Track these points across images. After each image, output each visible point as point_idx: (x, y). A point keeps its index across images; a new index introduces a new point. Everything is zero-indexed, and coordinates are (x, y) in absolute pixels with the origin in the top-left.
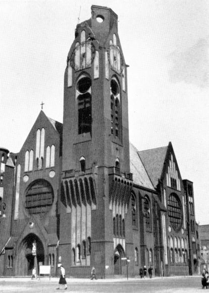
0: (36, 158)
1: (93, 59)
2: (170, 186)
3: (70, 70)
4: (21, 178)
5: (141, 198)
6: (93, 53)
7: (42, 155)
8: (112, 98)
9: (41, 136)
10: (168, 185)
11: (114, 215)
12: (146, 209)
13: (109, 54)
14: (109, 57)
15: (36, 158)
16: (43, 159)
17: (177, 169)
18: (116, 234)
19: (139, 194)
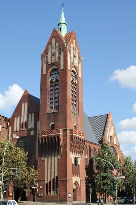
1: (59, 57)
2: (109, 141)
6: (60, 53)
7: (26, 119)
9: (25, 107)
13: (70, 53)
14: (71, 55)
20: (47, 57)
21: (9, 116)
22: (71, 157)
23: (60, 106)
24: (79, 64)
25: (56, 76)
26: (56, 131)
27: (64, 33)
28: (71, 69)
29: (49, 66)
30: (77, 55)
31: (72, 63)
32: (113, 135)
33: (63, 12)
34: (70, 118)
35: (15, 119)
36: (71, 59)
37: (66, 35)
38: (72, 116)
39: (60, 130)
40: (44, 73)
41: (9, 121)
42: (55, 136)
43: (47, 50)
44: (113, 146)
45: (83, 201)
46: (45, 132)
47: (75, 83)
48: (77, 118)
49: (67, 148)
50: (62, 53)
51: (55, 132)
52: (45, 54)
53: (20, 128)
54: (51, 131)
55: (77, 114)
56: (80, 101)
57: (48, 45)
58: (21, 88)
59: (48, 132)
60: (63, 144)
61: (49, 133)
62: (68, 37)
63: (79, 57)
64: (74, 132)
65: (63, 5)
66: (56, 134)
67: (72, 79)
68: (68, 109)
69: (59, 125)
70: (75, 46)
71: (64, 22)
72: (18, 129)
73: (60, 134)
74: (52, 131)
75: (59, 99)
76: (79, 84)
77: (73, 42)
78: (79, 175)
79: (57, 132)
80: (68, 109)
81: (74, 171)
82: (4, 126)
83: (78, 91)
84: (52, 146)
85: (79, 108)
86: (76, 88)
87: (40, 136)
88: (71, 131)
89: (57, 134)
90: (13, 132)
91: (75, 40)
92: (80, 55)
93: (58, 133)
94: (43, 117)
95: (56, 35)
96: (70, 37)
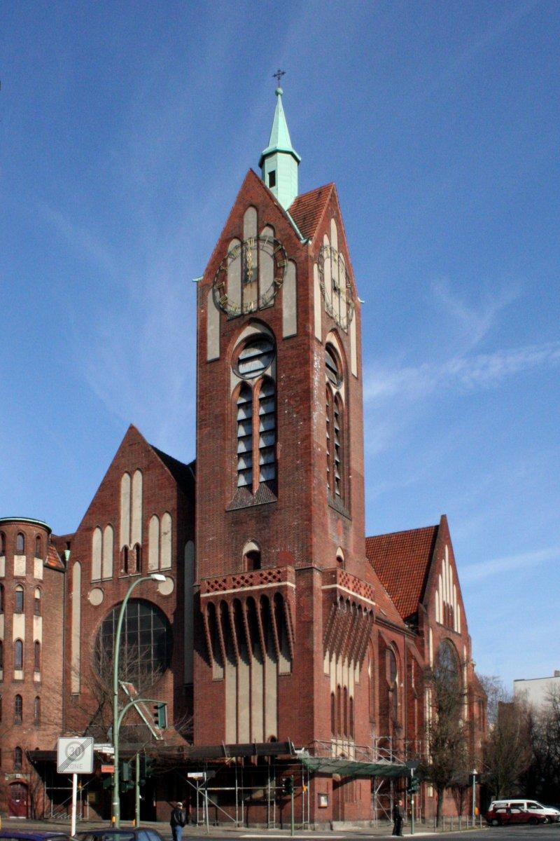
0: (121, 547)
1: (277, 287)
2: (442, 623)
3: (214, 317)
4: (84, 597)
5: (383, 648)
6: (279, 272)
7: (137, 539)
8: (329, 390)
9: (133, 488)
10: (437, 620)
11: (333, 688)
12: (393, 674)
13: (321, 272)
14: (322, 279)
15: (121, 547)
16: (141, 550)
17: (456, 581)
18: (336, 731)
19: (380, 637)
20: (223, 290)
21: (65, 526)
22: (326, 671)
23: (281, 480)
24: (349, 321)
25: (271, 379)
26: (270, 574)
27: (286, 193)
28: (324, 336)
29: (231, 323)
30: (342, 285)
31: (328, 316)
32: (453, 602)
33: (280, 106)
34: (323, 526)
35: (97, 534)
36: (323, 295)
37: (299, 201)
38: (329, 521)
39: (286, 571)
40: (213, 352)
41: (69, 544)
42: (267, 594)
43: (221, 257)
44: (451, 638)
45: (363, 820)
46: (225, 581)
47: (338, 393)
48: (346, 528)
49: (315, 638)
50: (291, 269)
51: (266, 578)
52: (216, 275)
53: (115, 571)
54: (247, 577)
55: (346, 513)
56: (353, 464)
57: (225, 242)
58: (175, 483)
59: (238, 578)
60: (299, 621)
61: (238, 583)
62: (313, 207)
63: (351, 293)
64: (339, 580)
65: (279, 75)
66: (271, 585)
67: (327, 380)
68: (316, 493)
69: (278, 553)
70: (335, 245)
71: (289, 147)
72: (108, 573)
73: (286, 587)
74: (251, 577)
75: (279, 453)
76: (351, 400)
77: (330, 231)
78: (352, 736)
79: (220, 586)
80: (316, 493)
81: (336, 709)
82: (52, 564)
83: (346, 426)
84: (260, 627)
85: (349, 493)
86: (340, 433)
87: (203, 595)
88: (331, 577)
89: (275, 584)
90: (87, 584)
91: (338, 224)
92: (352, 285)
93: (279, 581)
94: (209, 527)
95: (256, 192)
96: (318, 207)
